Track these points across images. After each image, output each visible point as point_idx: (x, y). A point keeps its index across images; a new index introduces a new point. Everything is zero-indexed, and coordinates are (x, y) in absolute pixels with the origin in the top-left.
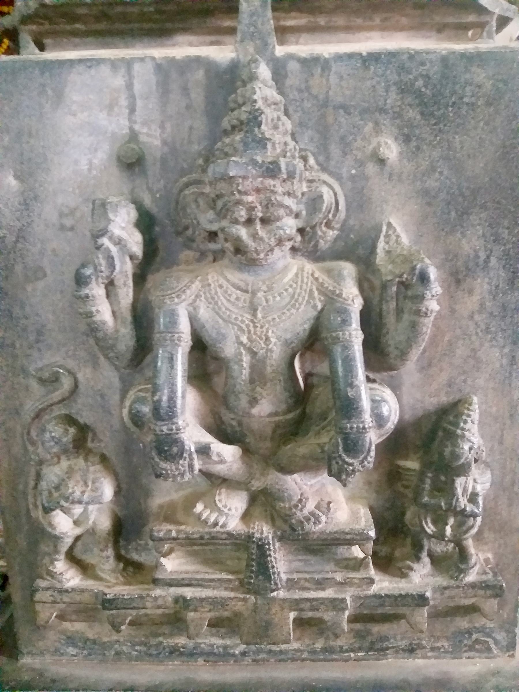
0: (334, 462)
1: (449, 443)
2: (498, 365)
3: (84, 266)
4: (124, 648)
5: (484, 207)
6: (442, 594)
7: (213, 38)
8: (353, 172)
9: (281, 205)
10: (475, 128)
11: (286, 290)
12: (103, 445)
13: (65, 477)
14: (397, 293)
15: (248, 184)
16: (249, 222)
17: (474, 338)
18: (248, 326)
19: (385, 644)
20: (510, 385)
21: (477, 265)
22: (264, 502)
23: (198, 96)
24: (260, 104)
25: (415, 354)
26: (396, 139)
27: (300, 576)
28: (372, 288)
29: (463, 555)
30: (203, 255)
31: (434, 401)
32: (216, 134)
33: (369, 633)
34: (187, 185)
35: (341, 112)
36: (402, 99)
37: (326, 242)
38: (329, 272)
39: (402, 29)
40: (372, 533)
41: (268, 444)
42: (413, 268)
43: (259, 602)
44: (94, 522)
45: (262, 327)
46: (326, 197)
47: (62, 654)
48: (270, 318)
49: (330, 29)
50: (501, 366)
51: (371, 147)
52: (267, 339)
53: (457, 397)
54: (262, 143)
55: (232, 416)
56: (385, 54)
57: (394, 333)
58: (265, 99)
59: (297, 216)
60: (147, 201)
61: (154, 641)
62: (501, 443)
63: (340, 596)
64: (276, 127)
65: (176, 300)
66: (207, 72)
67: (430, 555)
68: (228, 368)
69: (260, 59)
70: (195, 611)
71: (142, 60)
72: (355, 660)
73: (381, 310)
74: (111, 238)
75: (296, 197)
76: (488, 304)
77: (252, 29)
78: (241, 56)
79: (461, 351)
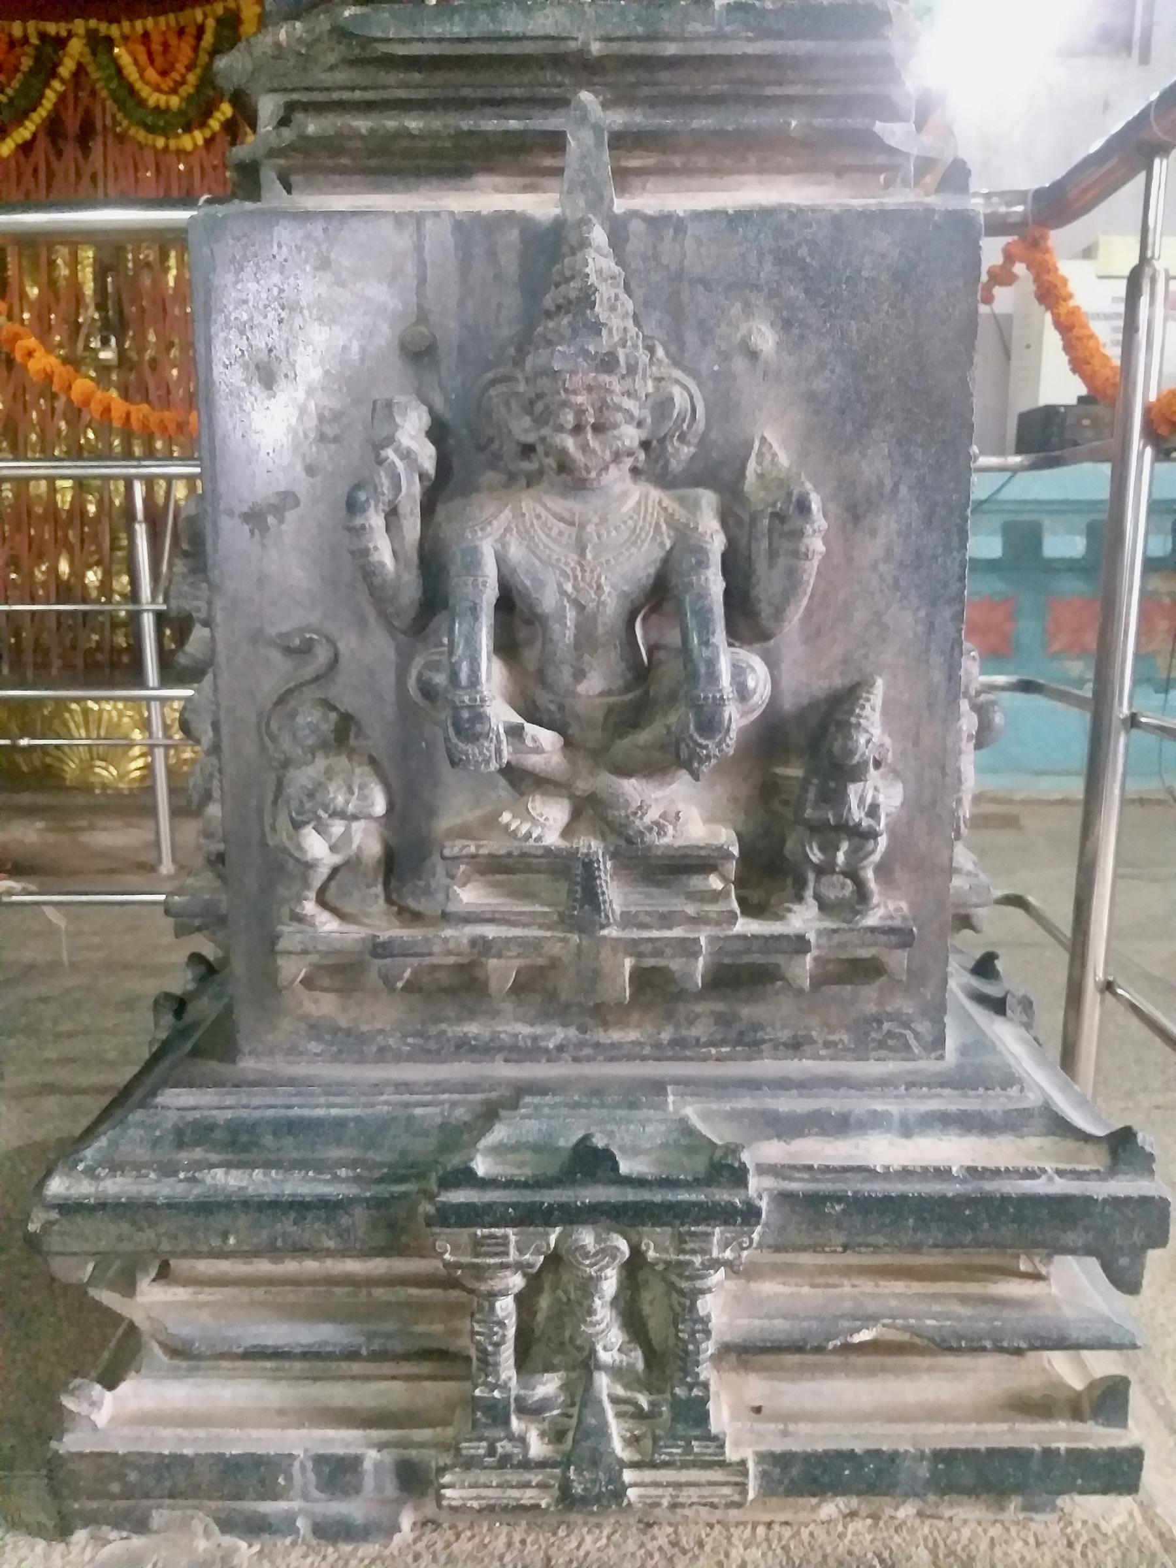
0: (683, 746)
1: (839, 736)
2: (911, 634)
3: (358, 487)
4: (391, 1041)
5: (890, 417)
6: (830, 939)
7: (527, 180)
8: (716, 368)
9: (619, 408)
10: (877, 312)
11: (625, 523)
12: (370, 743)
13: (323, 779)
14: (770, 530)
15: (577, 381)
16: (578, 429)
17: (878, 596)
18: (574, 570)
19: (760, 1034)
20: (927, 661)
21: (881, 495)
22: (589, 810)
23: (510, 263)
24: (593, 279)
25: (795, 615)
26: (772, 325)
27: (639, 909)
28: (739, 522)
29: (862, 895)
30: (512, 477)
31: (824, 684)
32: (533, 314)
33: (736, 1017)
34: (493, 383)
35: (700, 287)
36: (780, 272)
37: (679, 462)
38: (682, 501)
39: (787, 171)
40: (735, 850)
41: (598, 734)
42: (789, 494)
43: (585, 943)
44: (359, 847)
45: (592, 571)
46: (677, 400)
47: (301, 1054)
48: (603, 560)
49: (687, 171)
50: (916, 634)
51: (739, 335)
52: (599, 586)
53: (856, 678)
54: (596, 328)
55: (551, 697)
56: (758, 213)
57: (767, 584)
58: (600, 272)
59: (640, 424)
60: (438, 401)
61: (433, 1030)
62: (916, 742)
63: (692, 935)
64: (613, 308)
65: (480, 534)
66: (522, 232)
67: (817, 897)
68: (545, 629)
69: (594, 220)
70: (499, 956)
71: (437, 214)
72: (718, 1060)
73: (750, 550)
74: (396, 451)
75: (637, 398)
76: (897, 550)
77: (583, 176)
78: (568, 212)
79: (861, 615)
